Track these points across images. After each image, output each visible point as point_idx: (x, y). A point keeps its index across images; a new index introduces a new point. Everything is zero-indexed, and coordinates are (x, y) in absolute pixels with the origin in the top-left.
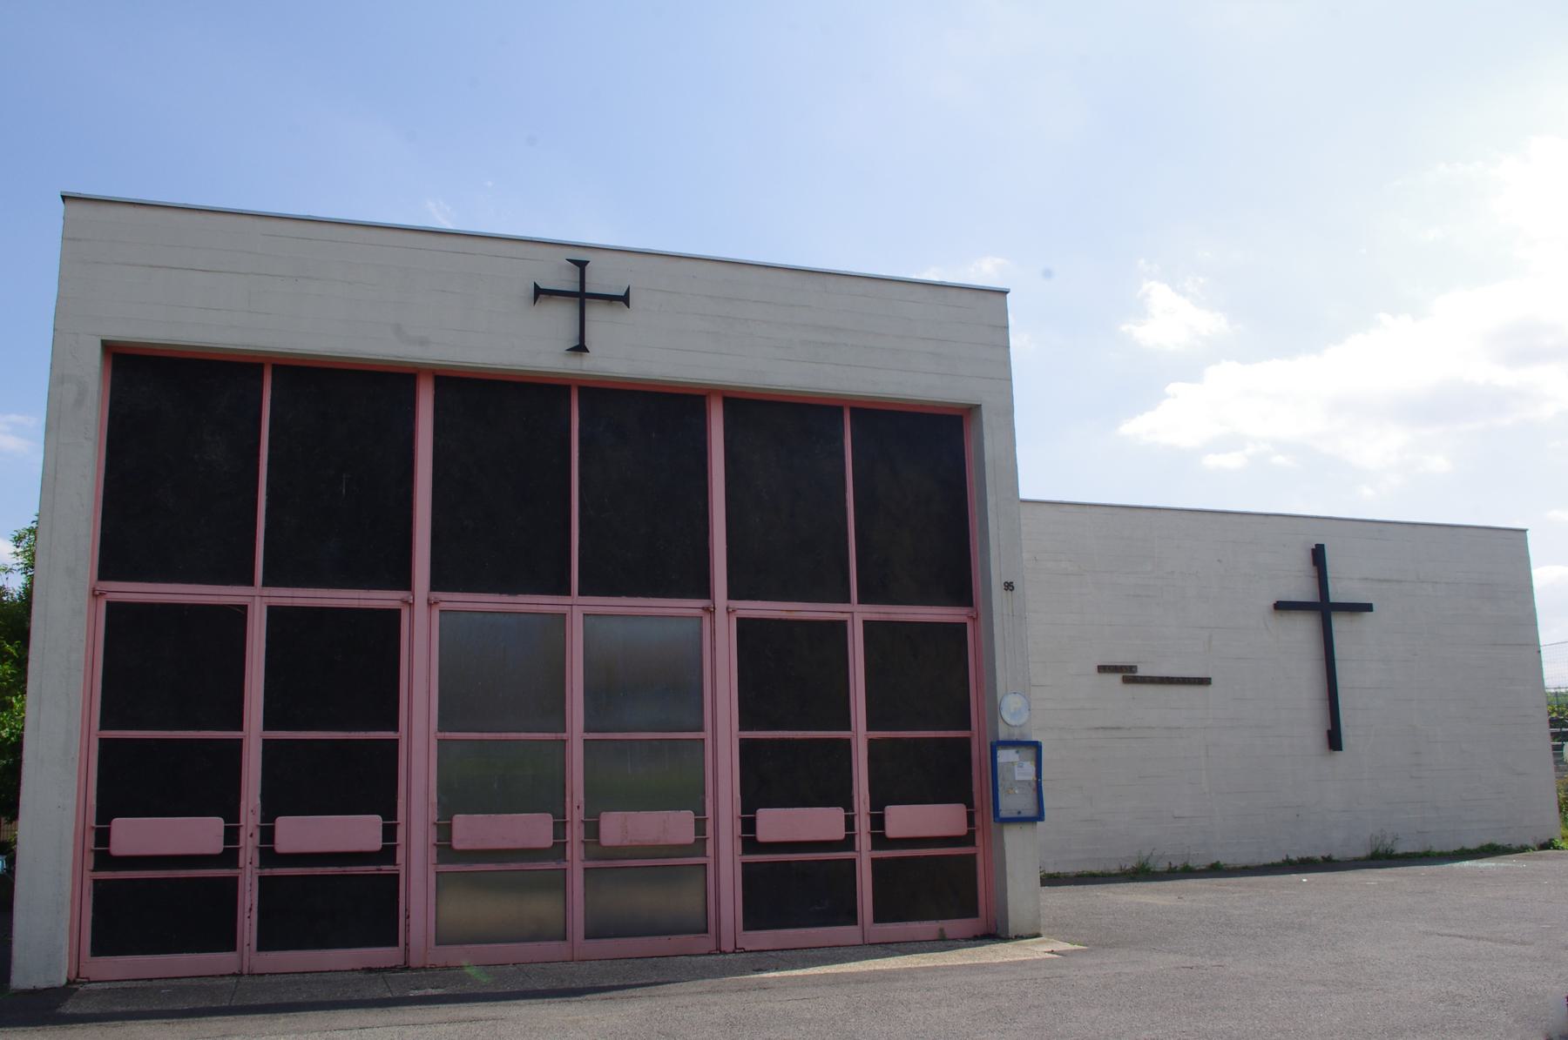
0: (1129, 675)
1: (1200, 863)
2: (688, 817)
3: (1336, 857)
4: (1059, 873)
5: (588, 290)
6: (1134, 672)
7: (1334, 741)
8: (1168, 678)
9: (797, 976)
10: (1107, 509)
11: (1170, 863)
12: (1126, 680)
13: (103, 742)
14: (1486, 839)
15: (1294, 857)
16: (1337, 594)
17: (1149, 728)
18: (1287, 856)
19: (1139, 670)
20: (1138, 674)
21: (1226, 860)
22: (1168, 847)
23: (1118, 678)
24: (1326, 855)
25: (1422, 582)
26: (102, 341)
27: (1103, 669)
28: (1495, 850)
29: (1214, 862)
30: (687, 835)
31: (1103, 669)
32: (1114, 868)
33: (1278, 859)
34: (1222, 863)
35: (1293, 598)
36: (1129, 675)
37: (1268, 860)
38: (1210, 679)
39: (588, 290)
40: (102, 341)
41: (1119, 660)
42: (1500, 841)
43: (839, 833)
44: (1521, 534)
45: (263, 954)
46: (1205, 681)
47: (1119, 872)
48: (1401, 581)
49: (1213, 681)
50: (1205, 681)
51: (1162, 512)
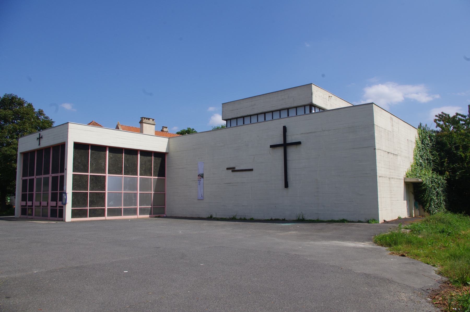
0: (233, 170)
1: (248, 218)
2: (46, 202)
3: (286, 219)
4: (328, 220)
5: (289, 140)
6: (234, 169)
7: (286, 186)
8: (242, 170)
9: (347, 247)
10: (336, 111)
11: (241, 217)
12: (233, 171)
13: (22, 194)
14: (341, 218)
15: (273, 218)
16: (281, 142)
17: (237, 183)
18: (241, 217)
19: (236, 168)
20: (236, 169)
21: (255, 217)
22: (241, 214)
23: (231, 171)
24: (283, 218)
25: (324, 131)
26: (74, 142)
27: (228, 169)
28: (334, 222)
29: (252, 218)
30: (55, 205)
31: (228, 169)
32: (228, 217)
33: (269, 218)
34: (254, 218)
35: (278, 143)
36: (233, 170)
37: (266, 218)
38: (283, 126)
39: (289, 140)
40: (74, 142)
41: (232, 166)
42: (345, 218)
43: (55, 205)
44: (370, 105)
45: (90, 218)
46: (251, 170)
47: (229, 218)
48: (316, 132)
49: (253, 169)
50: (251, 170)
51: (340, 109)
